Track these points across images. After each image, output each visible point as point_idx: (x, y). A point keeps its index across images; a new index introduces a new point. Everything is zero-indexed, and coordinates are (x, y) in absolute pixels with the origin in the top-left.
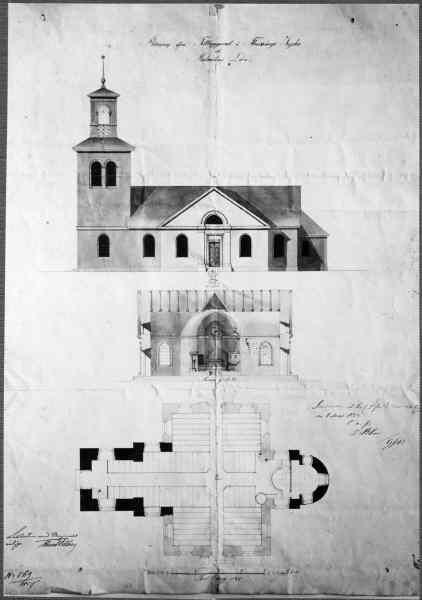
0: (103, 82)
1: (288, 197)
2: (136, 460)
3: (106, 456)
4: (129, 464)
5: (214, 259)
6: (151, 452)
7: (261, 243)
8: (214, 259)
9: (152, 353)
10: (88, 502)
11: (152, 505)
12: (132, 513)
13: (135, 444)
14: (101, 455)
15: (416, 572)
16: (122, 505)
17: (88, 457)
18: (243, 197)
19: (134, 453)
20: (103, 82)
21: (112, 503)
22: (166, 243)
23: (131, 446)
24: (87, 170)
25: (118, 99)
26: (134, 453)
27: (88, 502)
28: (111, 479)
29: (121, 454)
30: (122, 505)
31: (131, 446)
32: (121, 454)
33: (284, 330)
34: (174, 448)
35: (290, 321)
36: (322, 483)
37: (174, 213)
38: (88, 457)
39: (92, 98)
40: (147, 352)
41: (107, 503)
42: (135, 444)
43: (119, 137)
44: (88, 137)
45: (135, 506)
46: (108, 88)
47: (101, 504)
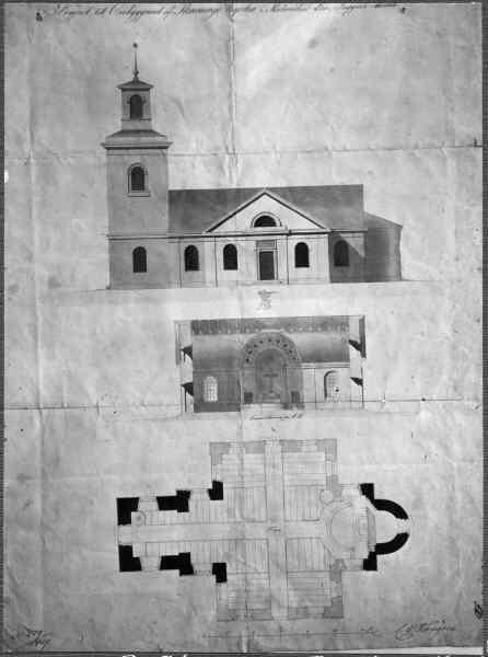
0: (136, 73)
1: (353, 194)
2: (180, 511)
3: (148, 506)
4: (172, 515)
5: (267, 269)
6: (198, 500)
7: (319, 251)
8: (267, 269)
9: (196, 389)
10: (129, 561)
11: (202, 561)
12: (177, 572)
13: (178, 492)
14: (141, 506)
15: (480, 623)
16: (168, 563)
17: (126, 508)
18: (296, 196)
19: (179, 502)
20: (136, 73)
21: (157, 562)
22: (210, 252)
23: (135, 556)
24: (123, 177)
25: (152, 91)
26: (179, 502)
27: (129, 561)
28: (159, 534)
29: (165, 503)
30: (168, 563)
31: (174, 494)
32: (165, 503)
33: (354, 352)
34: (123, 528)
35: (363, 338)
36: (402, 531)
37: (216, 218)
38: (126, 508)
39: (123, 90)
40: (189, 388)
41: (151, 562)
42: (178, 492)
43: (153, 128)
44: (119, 130)
45: (180, 563)
46: (140, 80)
47: (144, 564)
